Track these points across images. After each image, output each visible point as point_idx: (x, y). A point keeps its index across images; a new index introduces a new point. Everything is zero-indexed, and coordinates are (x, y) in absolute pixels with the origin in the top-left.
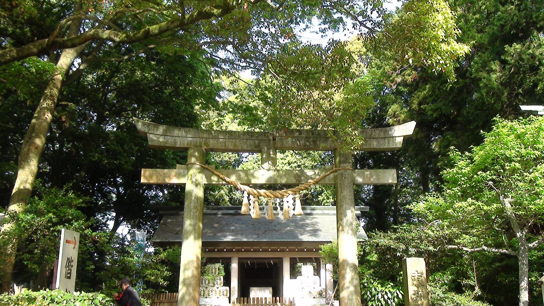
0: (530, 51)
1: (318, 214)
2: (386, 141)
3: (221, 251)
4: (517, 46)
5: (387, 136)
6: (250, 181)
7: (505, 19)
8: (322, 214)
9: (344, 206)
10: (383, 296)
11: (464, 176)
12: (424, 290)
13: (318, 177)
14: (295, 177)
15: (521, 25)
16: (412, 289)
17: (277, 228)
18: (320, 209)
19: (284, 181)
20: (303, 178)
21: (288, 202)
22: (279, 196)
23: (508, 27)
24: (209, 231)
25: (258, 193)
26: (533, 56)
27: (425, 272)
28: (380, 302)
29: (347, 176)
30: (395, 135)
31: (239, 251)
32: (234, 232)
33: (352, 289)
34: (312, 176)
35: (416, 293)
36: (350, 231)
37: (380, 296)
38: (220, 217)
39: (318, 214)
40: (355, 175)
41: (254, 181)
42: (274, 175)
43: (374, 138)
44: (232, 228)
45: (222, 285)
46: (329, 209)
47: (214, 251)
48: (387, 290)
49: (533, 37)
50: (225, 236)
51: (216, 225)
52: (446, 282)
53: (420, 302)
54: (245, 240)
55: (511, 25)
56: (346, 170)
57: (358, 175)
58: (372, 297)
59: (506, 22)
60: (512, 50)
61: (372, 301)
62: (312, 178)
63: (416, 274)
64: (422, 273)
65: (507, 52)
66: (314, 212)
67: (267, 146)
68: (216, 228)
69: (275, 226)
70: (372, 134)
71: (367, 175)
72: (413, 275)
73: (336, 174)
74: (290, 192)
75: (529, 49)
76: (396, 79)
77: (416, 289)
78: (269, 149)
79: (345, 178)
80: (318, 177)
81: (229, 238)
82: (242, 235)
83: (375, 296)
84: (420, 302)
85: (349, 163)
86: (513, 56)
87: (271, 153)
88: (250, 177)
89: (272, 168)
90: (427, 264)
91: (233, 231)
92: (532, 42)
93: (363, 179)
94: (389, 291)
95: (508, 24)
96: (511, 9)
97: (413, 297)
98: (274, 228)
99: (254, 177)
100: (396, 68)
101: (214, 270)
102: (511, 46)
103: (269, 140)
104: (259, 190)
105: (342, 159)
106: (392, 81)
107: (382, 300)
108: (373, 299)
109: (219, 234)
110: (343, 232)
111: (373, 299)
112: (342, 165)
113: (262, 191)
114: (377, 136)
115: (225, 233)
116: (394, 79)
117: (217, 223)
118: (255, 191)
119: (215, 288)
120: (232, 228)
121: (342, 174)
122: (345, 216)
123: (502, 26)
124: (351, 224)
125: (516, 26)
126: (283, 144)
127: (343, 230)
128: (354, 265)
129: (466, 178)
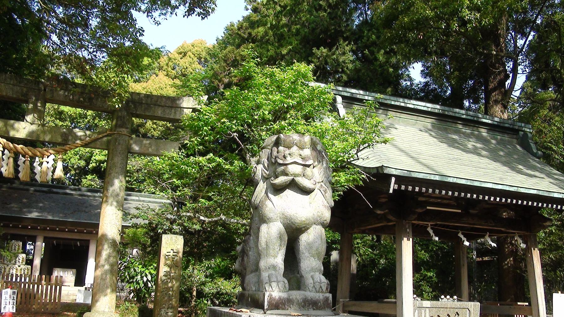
0: (335, 56)
1: (134, 200)
2: (173, 111)
3: (25, 227)
4: (324, 50)
5: (174, 105)
6: (8, 132)
7: (317, 23)
8: (137, 201)
9: (112, 175)
10: (142, 277)
11: (206, 125)
12: (177, 272)
13: (88, 139)
14: (62, 136)
15: (330, 31)
16: (163, 269)
17: (87, 210)
18: (136, 196)
19: (47, 138)
20: (70, 138)
21: (48, 163)
22: (38, 154)
23: (318, 31)
24: (16, 206)
25: (15, 147)
26: (337, 61)
27: (181, 250)
28: (139, 284)
29: (121, 142)
30: (182, 106)
31: (45, 229)
32: (41, 210)
33: (107, 267)
34: (82, 137)
35: (167, 274)
36: (115, 203)
37: (139, 277)
38: (32, 194)
39: (134, 200)
40: (131, 142)
41: (12, 133)
42: (38, 130)
43: (159, 106)
44: (41, 205)
45: (24, 263)
46: (145, 197)
47: (9, 227)
48: (147, 272)
49: (340, 45)
50: (31, 212)
51: (25, 200)
52: (213, 265)
53: (170, 285)
54: (50, 218)
55: (321, 30)
56: (120, 135)
57: (135, 143)
58: (130, 278)
59: (317, 26)
60: (318, 53)
61: (131, 283)
62: (81, 140)
63: (171, 254)
64: (178, 253)
65: (314, 54)
66: (129, 198)
67: (35, 96)
68: (24, 203)
69: (86, 207)
70: (157, 101)
71: (146, 144)
72: (168, 254)
73: (109, 138)
74: (51, 151)
75: (334, 54)
76: (224, 79)
77: (168, 270)
78: (37, 100)
79: (119, 144)
80: (88, 139)
81: (34, 215)
82: (49, 213)
83: (133, 277)
84: (170, 285)
85: (127, 128)
86: (319, 58)
87: (39, 105)
88: (9, 128)
89: (37, 122)
90: (185, 244)
91: (41, 208)
92: (337, 49)
93: (140, 148)
94: (150, 273)
95: (318, 28)
96: (323, 16)
97: (164, 278)
98: (84, 209)
99: (13, 129)
100: (225, 69)
101: (17, 247)
102: (318, 49)
103: (40, 90)
104: (16, 145)
105: (119, 123)
106: (220, 81)
107: (141, 282)
108: (132, 280)
109: (25, 210)
110: (107, 203)
111: (132, 280)
112: (118, 129)
113: (20, 147)
114: (163, 104)
115: (32, 209)
116: (221, 78)
117: (26, 199)
118: (11, 145)
119: (17, 266)
120: (41, 205)
121: (116, 139)
122: (112, 185)
123: (314, 29)
124: (118, 195)
125: (326, 31)
126: (53, 96)
127: (106, 201)
128: (114, 241)
129: (210, 127)
